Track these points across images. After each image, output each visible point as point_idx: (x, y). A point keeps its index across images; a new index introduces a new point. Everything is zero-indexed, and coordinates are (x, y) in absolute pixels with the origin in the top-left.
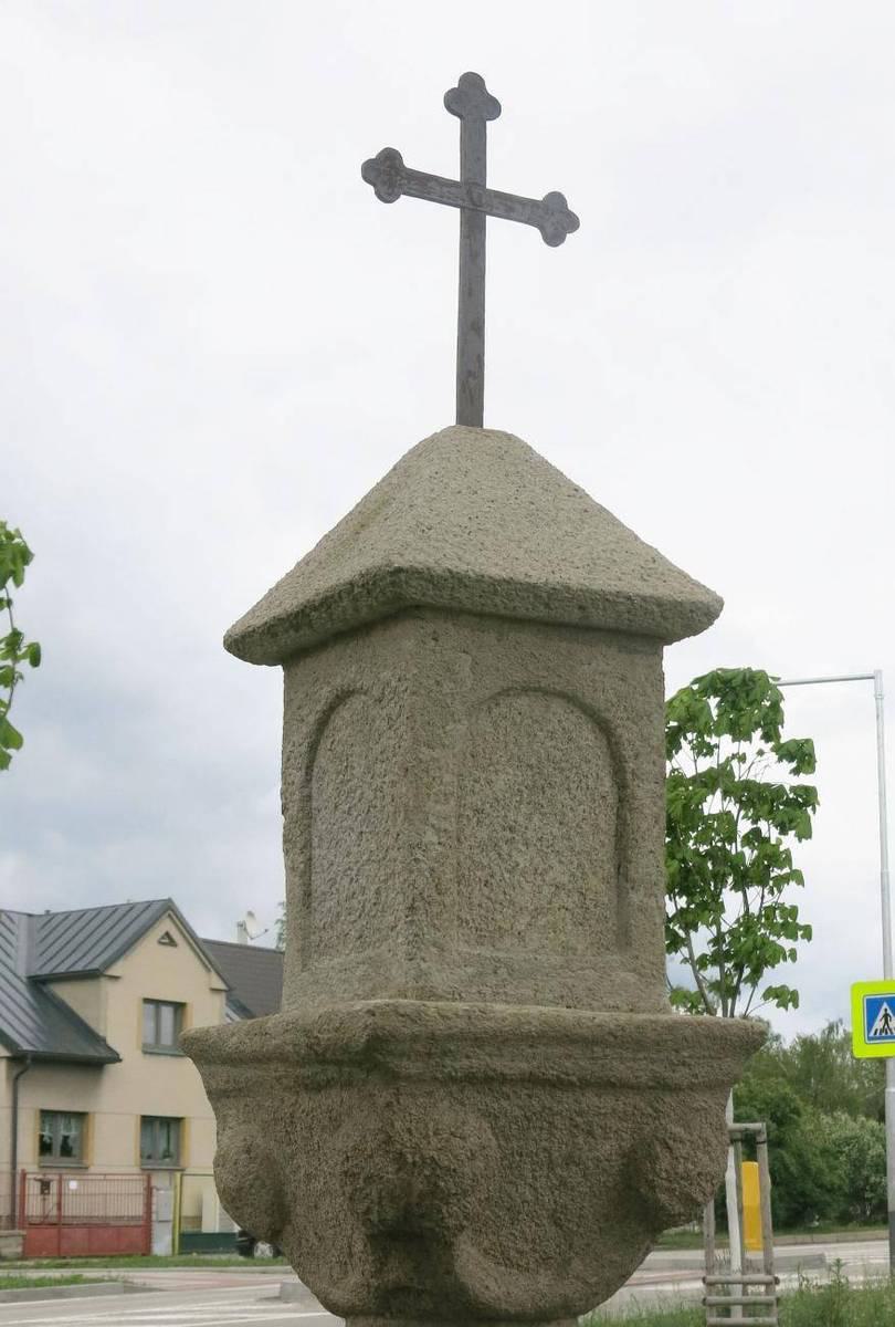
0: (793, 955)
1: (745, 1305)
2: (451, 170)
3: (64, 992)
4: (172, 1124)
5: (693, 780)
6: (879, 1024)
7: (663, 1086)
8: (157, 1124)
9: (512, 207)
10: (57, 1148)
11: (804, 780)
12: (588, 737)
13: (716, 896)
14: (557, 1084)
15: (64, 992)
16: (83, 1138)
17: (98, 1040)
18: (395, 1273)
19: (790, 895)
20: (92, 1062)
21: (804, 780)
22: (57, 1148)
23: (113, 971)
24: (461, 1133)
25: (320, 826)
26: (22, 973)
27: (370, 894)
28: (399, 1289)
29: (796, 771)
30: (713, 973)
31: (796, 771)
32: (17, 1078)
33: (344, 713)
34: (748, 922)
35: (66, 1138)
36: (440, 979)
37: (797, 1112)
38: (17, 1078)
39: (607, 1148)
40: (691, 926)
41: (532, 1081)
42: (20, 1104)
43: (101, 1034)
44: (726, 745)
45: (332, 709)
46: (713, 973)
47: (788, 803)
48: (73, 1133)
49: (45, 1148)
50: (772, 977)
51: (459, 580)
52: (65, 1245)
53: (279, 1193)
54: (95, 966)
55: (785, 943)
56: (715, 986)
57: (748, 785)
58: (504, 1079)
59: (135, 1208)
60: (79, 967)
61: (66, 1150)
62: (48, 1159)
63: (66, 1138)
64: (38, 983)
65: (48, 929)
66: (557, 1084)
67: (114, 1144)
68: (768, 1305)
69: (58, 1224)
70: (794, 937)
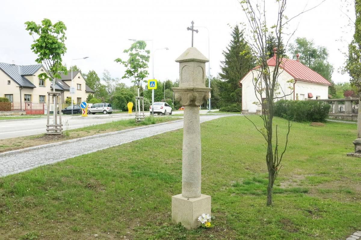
0: (147, 76)
1: (140, 118)
2: (194, 32)
3: (26, 77)
4: (44, 96)
5: (135, 54)
6: (151, 85)
7: (206, 92)
8: (42, 96)
9: (195, 30)
10: (27, 100)
11: (148, 55)
12: (202, 69)
13: (138, 69)
14: (201, 92)
15: (26, 77)
16: (31, 98)
17: (32, 84)
18: (191, 103)
19: (146, 69)
20: (32, 88)
21: (148, 55)
22: (27, 100)
23: (34, 75)
24: (196, 94)
25: (183, 74)
26: (20, 75)
27: (188, 79)
28: (191, 104)
29: (148, 54)
30: (137, 79)
31: (148, 54)
32: (21, 90)
33: (185, 67)
34: (141, 73)
35: (28, 98)
36: (195, 85)
37: (133, 96)
38: (21, 90)
39: (203, 96)
40: (134, 73)
41: (200, 91)
42: (21, 93)
43: (33, 83)
44: (139, 50)
45: (184, 66)
46: (137, 79)
47: (146, 58)
48: (29, 98)
49: (25, 100)
50: (144, 79)
51: (196, 59)
52: (32, 113)
53: (181, 98)
54: (31, 74)
55: (146, 75)
56: (138, 80)
57: (142, 55)
58: (199, 91)
59: (42, 108)
60: (29, 74)
61: (28, 100)
62: (26, 101)
63: (28, 98)
64: (23, 76)
65: (23, 68)
66: (201, 92)
67: (35, 99)
68: (143, 118)
69: (31, 111)
70: (147, 74)
